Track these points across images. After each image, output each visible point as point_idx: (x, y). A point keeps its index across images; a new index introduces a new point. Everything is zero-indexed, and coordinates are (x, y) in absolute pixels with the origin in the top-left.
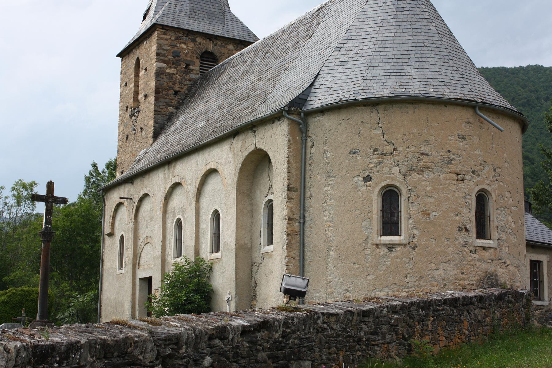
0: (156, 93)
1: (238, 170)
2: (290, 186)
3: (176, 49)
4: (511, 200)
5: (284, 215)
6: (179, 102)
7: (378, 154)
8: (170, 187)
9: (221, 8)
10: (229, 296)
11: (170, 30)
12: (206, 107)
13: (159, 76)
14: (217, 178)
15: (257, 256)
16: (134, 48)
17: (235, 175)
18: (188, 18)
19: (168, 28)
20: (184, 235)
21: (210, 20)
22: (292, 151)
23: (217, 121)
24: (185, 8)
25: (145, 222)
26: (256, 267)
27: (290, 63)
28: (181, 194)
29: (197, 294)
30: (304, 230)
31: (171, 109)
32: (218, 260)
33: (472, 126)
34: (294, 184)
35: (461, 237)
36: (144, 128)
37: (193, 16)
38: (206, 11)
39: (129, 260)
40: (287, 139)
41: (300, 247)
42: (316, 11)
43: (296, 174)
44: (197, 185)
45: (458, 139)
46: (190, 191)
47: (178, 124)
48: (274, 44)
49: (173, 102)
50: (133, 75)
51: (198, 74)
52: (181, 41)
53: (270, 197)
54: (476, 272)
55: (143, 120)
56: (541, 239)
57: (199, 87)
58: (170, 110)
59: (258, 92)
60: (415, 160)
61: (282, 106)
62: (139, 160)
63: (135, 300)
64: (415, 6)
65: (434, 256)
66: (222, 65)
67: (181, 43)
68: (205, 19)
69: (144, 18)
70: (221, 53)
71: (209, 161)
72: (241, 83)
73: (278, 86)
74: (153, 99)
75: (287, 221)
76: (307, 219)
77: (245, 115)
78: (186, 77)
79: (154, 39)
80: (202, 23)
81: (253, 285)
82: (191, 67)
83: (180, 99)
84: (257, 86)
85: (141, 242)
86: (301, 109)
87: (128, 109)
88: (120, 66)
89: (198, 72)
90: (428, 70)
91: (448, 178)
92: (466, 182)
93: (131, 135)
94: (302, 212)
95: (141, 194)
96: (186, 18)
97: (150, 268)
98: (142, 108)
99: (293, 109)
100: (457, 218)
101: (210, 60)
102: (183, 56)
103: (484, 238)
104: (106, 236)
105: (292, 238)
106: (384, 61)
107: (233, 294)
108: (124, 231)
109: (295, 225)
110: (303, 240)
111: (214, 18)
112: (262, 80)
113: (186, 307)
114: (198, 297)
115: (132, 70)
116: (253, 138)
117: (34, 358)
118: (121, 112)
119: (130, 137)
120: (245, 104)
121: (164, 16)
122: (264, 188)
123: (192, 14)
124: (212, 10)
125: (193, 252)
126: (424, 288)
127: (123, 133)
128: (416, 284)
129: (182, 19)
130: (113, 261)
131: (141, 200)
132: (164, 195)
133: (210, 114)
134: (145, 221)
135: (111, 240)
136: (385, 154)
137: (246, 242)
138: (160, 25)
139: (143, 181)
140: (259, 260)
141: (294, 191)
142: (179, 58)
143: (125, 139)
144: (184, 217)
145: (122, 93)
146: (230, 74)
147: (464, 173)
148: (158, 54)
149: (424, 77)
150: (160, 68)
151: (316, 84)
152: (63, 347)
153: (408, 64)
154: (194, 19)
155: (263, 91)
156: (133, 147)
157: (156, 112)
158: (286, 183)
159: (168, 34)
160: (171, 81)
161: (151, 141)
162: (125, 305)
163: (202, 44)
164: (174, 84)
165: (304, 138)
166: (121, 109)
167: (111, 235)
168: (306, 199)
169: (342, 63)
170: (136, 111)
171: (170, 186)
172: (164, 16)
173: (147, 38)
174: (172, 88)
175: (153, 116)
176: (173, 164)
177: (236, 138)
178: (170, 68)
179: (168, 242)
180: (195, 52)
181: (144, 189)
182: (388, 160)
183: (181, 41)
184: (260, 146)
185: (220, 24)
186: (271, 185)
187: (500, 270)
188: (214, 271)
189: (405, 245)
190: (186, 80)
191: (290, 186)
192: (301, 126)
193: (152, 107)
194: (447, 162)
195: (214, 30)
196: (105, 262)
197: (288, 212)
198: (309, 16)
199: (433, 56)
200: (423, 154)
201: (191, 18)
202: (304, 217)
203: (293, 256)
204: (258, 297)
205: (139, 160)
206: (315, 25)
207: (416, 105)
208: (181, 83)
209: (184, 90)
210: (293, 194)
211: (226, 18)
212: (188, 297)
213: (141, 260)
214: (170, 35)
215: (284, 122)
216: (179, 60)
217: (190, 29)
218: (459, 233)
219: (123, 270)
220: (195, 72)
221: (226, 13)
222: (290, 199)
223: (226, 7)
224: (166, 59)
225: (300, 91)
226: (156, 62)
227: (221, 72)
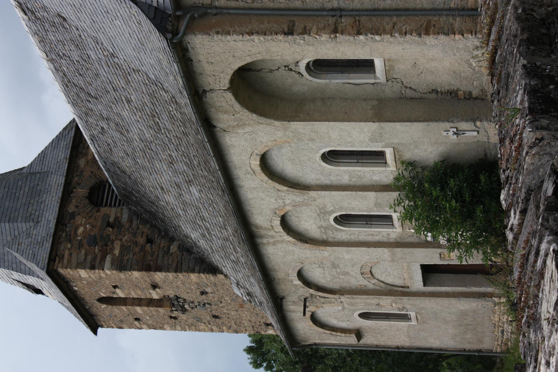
0: (150, 270)
1: (262, 120)
2: (286, 30)
3: (85, 241)
5: (330, 40)
6: (163, 237)
8: (288, 234)
9: (25, 178)
10: (451, 133)
12: (171, 189)
13: (125, 266)
14: (274, 156)
15: (391, 90)
16: (83, 306)
17: (269, 124)
18: (39, 224)
19: (54, 252)
20: (359, 211)
21: (42, 193)
22: (233, 29)
23: (190, 165)
24: (25, 229)
25: (341, 277)
26: (408, 91)
27: (104, 49)
28: (298, 217)
29: (448, 185)
30: (352, 10)
31: (174, 248)
32: (396, 153)
34: (283, 26)
36: (202, 290)
37: (36, 217)
38: (29, 199)
39: (396, 304)
40: (215, 36)
41: (378, 15)
42: (26, 14)
43: (268, 23)
44: (285, 188)
46: (293, 201)
47: (194, 235)
48: (76, 82)
49: (162, 245)
50: (124, 308)
51: (122, 209)
52: (73, 233)
53: (302, 67)
55: (190, 291)
57: (142, 207)
58: (174, 250)
59: (147, 99)
61: (165, 44)
62: (249, 294)
63: (456, 293)
66: (108, 171)
67: (76, 234)
68: (40, 200)
69: (38, 291)
70: (90, 177)
71: (249, 169)
72: (134, 133)
73: (137, 63)
74: (159, 274)
75: (338, 35)
77: (181, 113)
78: (126, 227)
79: (69, 273)
80: (46, 205)
81: (434, 96)
82: (111, 219)
83: (159, 235)
84: (138, 103)
85: (370, 284)
86: (170, 15)
87: (173, 315)
88: (110, 329)
89: (119, 210)
93: (211, 311)
94: (325, 13)
95: (298, 282)
96: (39, 227)
97: (409, 268)
98: (172, 292)
99: (169, 27)
102: (96, 231)
104: (361, 342)
105: (364, 27)
107: (447, 125)
108: (354, 311)
109: (344, 24)
110: (367, 10)
111: (39, 188)
112: (129, 96)
113: (467, 199)
114: (452, 182)
115: (118, 311)
116: (214, 95)
117: (551, 112)
118: (178, 327)
119: (214, 313)
120: (165, 121)
121: (35, 260)
122: (290, 79)
123: (33, 219)
124: (27, 190)
125: (385, 194)
127: (210, 324)
129: (40, 234)
130: (398, 331)
131: (307, 283)
132: (299, 244)
133: (180, 179)
134: (339, 278)
135: (366, 334)
137: (369, 108)
138: (49, 264)
139: (279, 279)
140: (397, 87)
141: (294, 26)
142: (98, 237)
143: (217, 320)
144: (333, 212)
145: (150, 327)
146: (122, 154)
148: (93, 268)
150: (112, 264)
152: (532, 83)
154: (40, 215)
155: (144, 89)
156: (230, 307)
157: (178, 270)
158: (281, 37)
159: (62, 252)
160: (132, 248)
161: (221, 277)
162: (464, 308)
163: (77, 204)
164: (136, 243)
165: (214, 11)
166: (173, 328)
167: (359, 334)
168: (305, 7)
170: (176, 303)
171: (286, 234)
172: (35, 260)
173: (68, 286)
174: (143, 248)
175: (184, 274)
176: (254, 229)
177: (215, 123)
178: (112, 249)
179: (370, 239)
180: (90, 215)
181: (290, 278)
183: (73, 233)
184: (226, 83)
185: (49, 178)
186: (285, 66)
188: (413, 158)
190: (131, 226)
191: (286, 30)
192: (196, 15)
193: (171, 275)
195: (56, 187)
196: (399, 344)
197: (325, 33)
198: (34, 27)
201: (39, 220)
202: (332, 10)
203: (391, 25)
204: (452, 87)
205: (249, 294)
206: (45, 14)
208: (135, 234)
209: (146, 229)
210: (299, 26)
211: (40, 171)
212: (453, 197)
213: (396, 284)
214: (64, 250)
215: (190, 41)
217: (55, 221)
219: (411, 313)
220: (119, 214)
221: (31, 171)
222: (305, 31)
223: (22, 172)
224: (99, 255)
225: (143, 18)
226: (103, 270)
227: (119, 172)
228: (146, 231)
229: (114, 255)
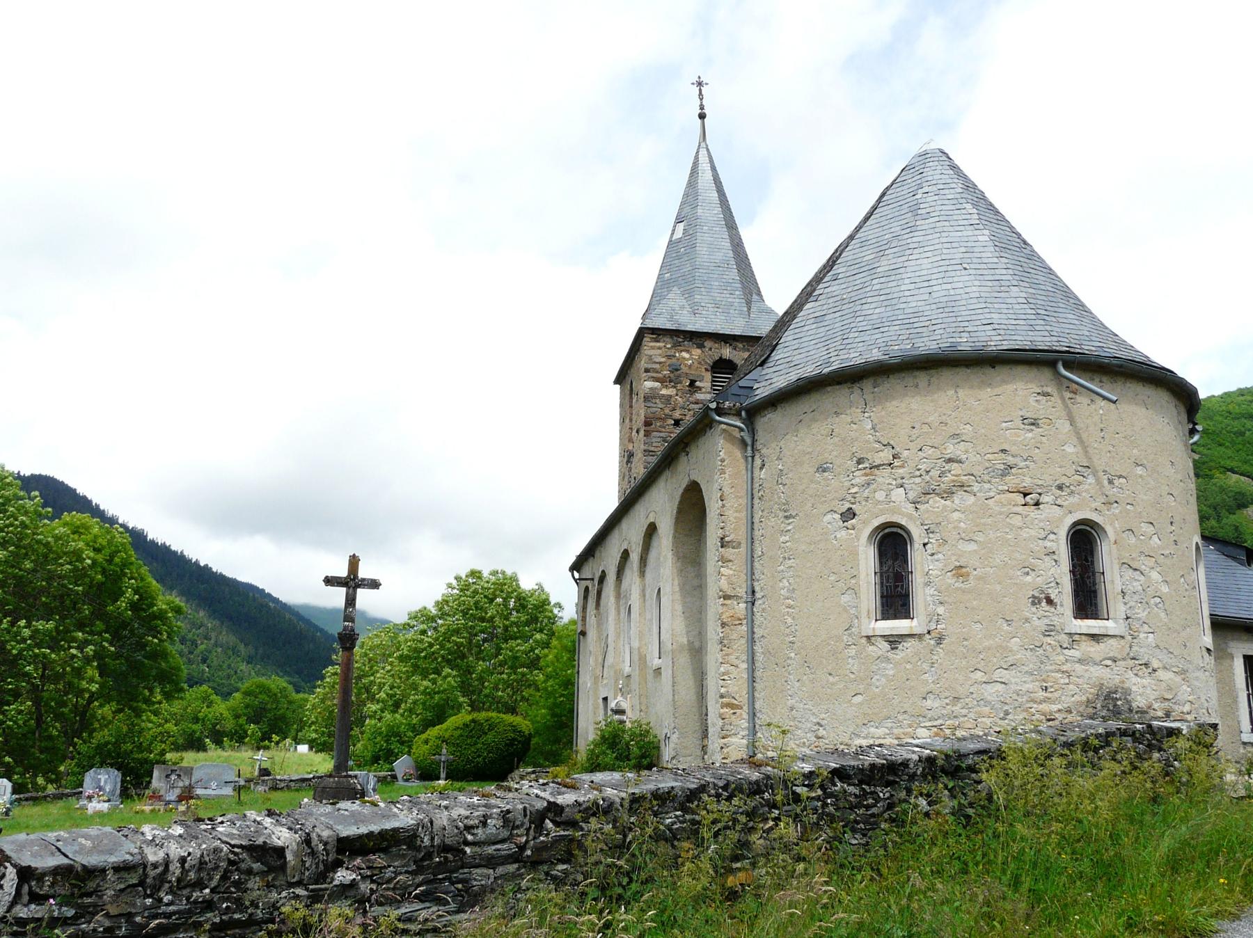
3: (674, 360)
4: (1157, 540)
7: (865, 468)
11: (664, 335)
33: (1052, 398)
35: (1039, 618)
45: (1023, 426)
51: (710, 393)
54: (1077, 685)
56: (1244, 612)
60: (934, 473)
64: (953, 207)
65: (982, 657)
67: (683, 351)
76: (758, 595)
82: (698, 384)
89: (709, 390)
90: (964, 308)
91: (1005, 503)
92: (1044, 507)
100: (1029, 579)
101: (728, 371)
102: (684, 369)
103: (1095, 616)
106: (885, 303)
124: (729, 300)
126: (962, 719)
128: (944, 712)
136: (877, 467)
147: (1040, 491)
149: (954, 319)
151: (771, 360)
153: (927, 302)
169: (818, 320)
182: (883, 476)
187: (1135, 680)
189: (920, 637)
194: (1000, 472)
199: (977, 283)
200: (950, 460)
207: (933, 371)
216: (679, 376)
218: (1034, 609)
220: (704, 390)
224: (660, 375)
228: (687, 418)
229: (661, 390)
